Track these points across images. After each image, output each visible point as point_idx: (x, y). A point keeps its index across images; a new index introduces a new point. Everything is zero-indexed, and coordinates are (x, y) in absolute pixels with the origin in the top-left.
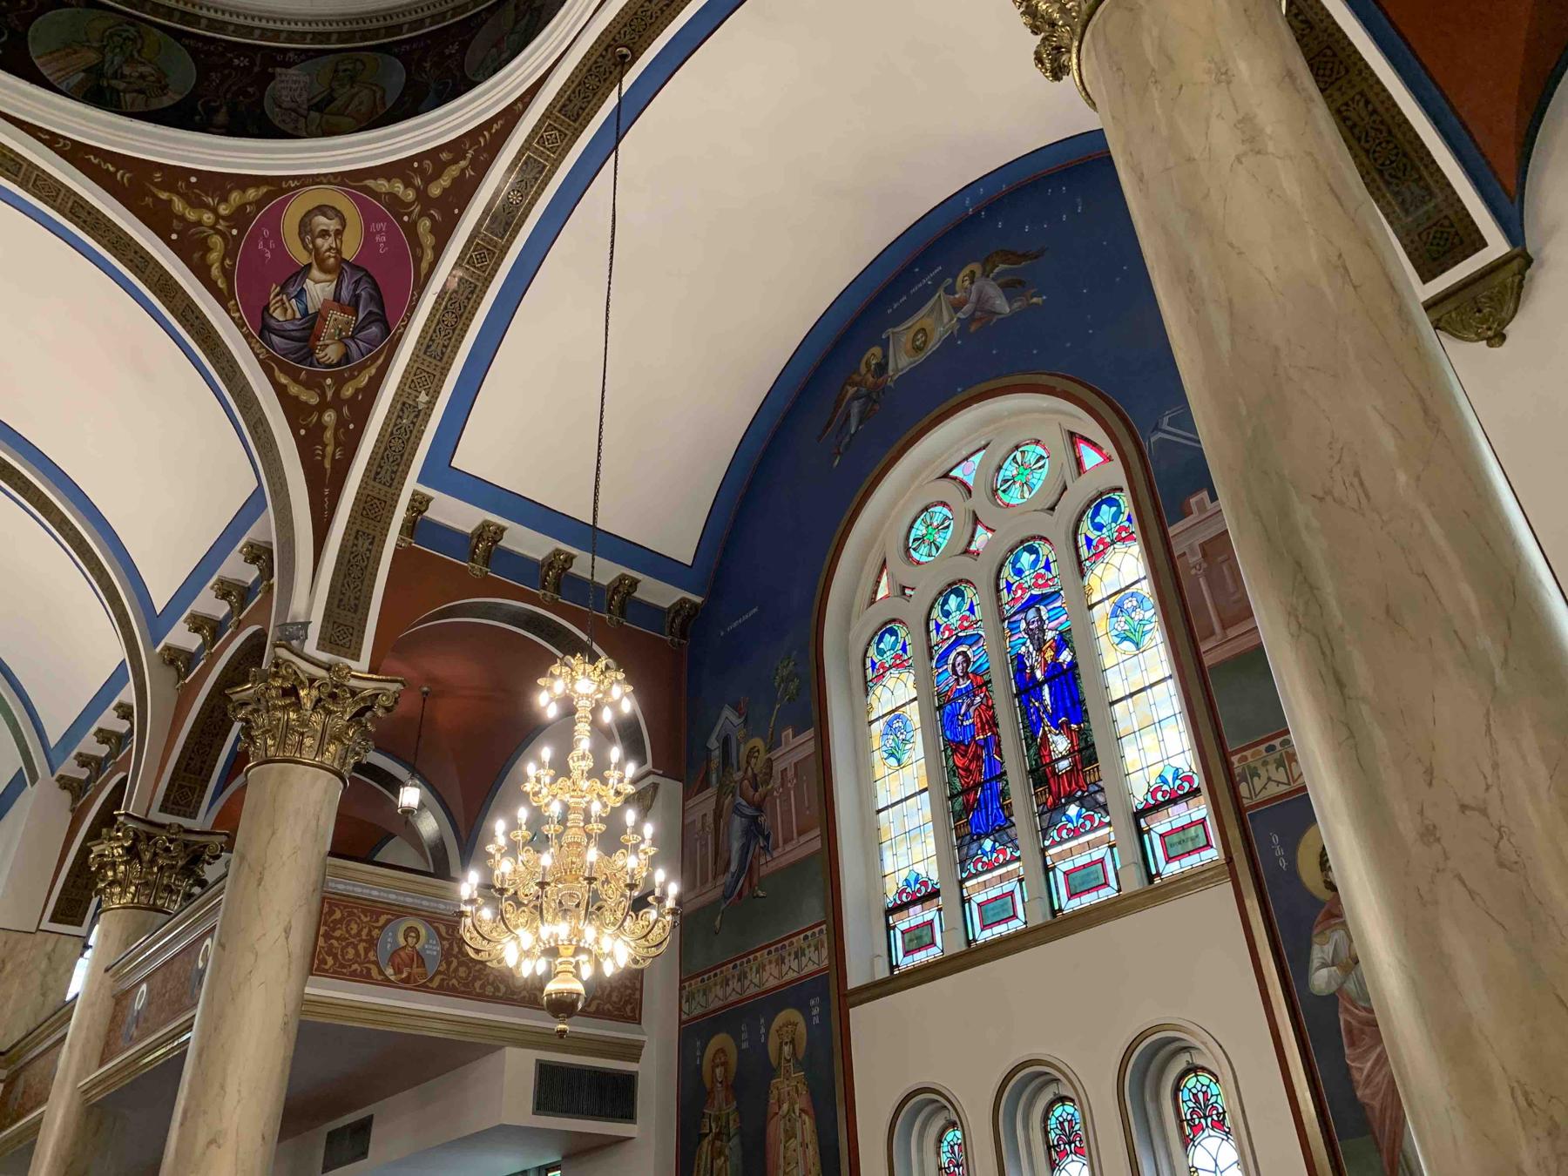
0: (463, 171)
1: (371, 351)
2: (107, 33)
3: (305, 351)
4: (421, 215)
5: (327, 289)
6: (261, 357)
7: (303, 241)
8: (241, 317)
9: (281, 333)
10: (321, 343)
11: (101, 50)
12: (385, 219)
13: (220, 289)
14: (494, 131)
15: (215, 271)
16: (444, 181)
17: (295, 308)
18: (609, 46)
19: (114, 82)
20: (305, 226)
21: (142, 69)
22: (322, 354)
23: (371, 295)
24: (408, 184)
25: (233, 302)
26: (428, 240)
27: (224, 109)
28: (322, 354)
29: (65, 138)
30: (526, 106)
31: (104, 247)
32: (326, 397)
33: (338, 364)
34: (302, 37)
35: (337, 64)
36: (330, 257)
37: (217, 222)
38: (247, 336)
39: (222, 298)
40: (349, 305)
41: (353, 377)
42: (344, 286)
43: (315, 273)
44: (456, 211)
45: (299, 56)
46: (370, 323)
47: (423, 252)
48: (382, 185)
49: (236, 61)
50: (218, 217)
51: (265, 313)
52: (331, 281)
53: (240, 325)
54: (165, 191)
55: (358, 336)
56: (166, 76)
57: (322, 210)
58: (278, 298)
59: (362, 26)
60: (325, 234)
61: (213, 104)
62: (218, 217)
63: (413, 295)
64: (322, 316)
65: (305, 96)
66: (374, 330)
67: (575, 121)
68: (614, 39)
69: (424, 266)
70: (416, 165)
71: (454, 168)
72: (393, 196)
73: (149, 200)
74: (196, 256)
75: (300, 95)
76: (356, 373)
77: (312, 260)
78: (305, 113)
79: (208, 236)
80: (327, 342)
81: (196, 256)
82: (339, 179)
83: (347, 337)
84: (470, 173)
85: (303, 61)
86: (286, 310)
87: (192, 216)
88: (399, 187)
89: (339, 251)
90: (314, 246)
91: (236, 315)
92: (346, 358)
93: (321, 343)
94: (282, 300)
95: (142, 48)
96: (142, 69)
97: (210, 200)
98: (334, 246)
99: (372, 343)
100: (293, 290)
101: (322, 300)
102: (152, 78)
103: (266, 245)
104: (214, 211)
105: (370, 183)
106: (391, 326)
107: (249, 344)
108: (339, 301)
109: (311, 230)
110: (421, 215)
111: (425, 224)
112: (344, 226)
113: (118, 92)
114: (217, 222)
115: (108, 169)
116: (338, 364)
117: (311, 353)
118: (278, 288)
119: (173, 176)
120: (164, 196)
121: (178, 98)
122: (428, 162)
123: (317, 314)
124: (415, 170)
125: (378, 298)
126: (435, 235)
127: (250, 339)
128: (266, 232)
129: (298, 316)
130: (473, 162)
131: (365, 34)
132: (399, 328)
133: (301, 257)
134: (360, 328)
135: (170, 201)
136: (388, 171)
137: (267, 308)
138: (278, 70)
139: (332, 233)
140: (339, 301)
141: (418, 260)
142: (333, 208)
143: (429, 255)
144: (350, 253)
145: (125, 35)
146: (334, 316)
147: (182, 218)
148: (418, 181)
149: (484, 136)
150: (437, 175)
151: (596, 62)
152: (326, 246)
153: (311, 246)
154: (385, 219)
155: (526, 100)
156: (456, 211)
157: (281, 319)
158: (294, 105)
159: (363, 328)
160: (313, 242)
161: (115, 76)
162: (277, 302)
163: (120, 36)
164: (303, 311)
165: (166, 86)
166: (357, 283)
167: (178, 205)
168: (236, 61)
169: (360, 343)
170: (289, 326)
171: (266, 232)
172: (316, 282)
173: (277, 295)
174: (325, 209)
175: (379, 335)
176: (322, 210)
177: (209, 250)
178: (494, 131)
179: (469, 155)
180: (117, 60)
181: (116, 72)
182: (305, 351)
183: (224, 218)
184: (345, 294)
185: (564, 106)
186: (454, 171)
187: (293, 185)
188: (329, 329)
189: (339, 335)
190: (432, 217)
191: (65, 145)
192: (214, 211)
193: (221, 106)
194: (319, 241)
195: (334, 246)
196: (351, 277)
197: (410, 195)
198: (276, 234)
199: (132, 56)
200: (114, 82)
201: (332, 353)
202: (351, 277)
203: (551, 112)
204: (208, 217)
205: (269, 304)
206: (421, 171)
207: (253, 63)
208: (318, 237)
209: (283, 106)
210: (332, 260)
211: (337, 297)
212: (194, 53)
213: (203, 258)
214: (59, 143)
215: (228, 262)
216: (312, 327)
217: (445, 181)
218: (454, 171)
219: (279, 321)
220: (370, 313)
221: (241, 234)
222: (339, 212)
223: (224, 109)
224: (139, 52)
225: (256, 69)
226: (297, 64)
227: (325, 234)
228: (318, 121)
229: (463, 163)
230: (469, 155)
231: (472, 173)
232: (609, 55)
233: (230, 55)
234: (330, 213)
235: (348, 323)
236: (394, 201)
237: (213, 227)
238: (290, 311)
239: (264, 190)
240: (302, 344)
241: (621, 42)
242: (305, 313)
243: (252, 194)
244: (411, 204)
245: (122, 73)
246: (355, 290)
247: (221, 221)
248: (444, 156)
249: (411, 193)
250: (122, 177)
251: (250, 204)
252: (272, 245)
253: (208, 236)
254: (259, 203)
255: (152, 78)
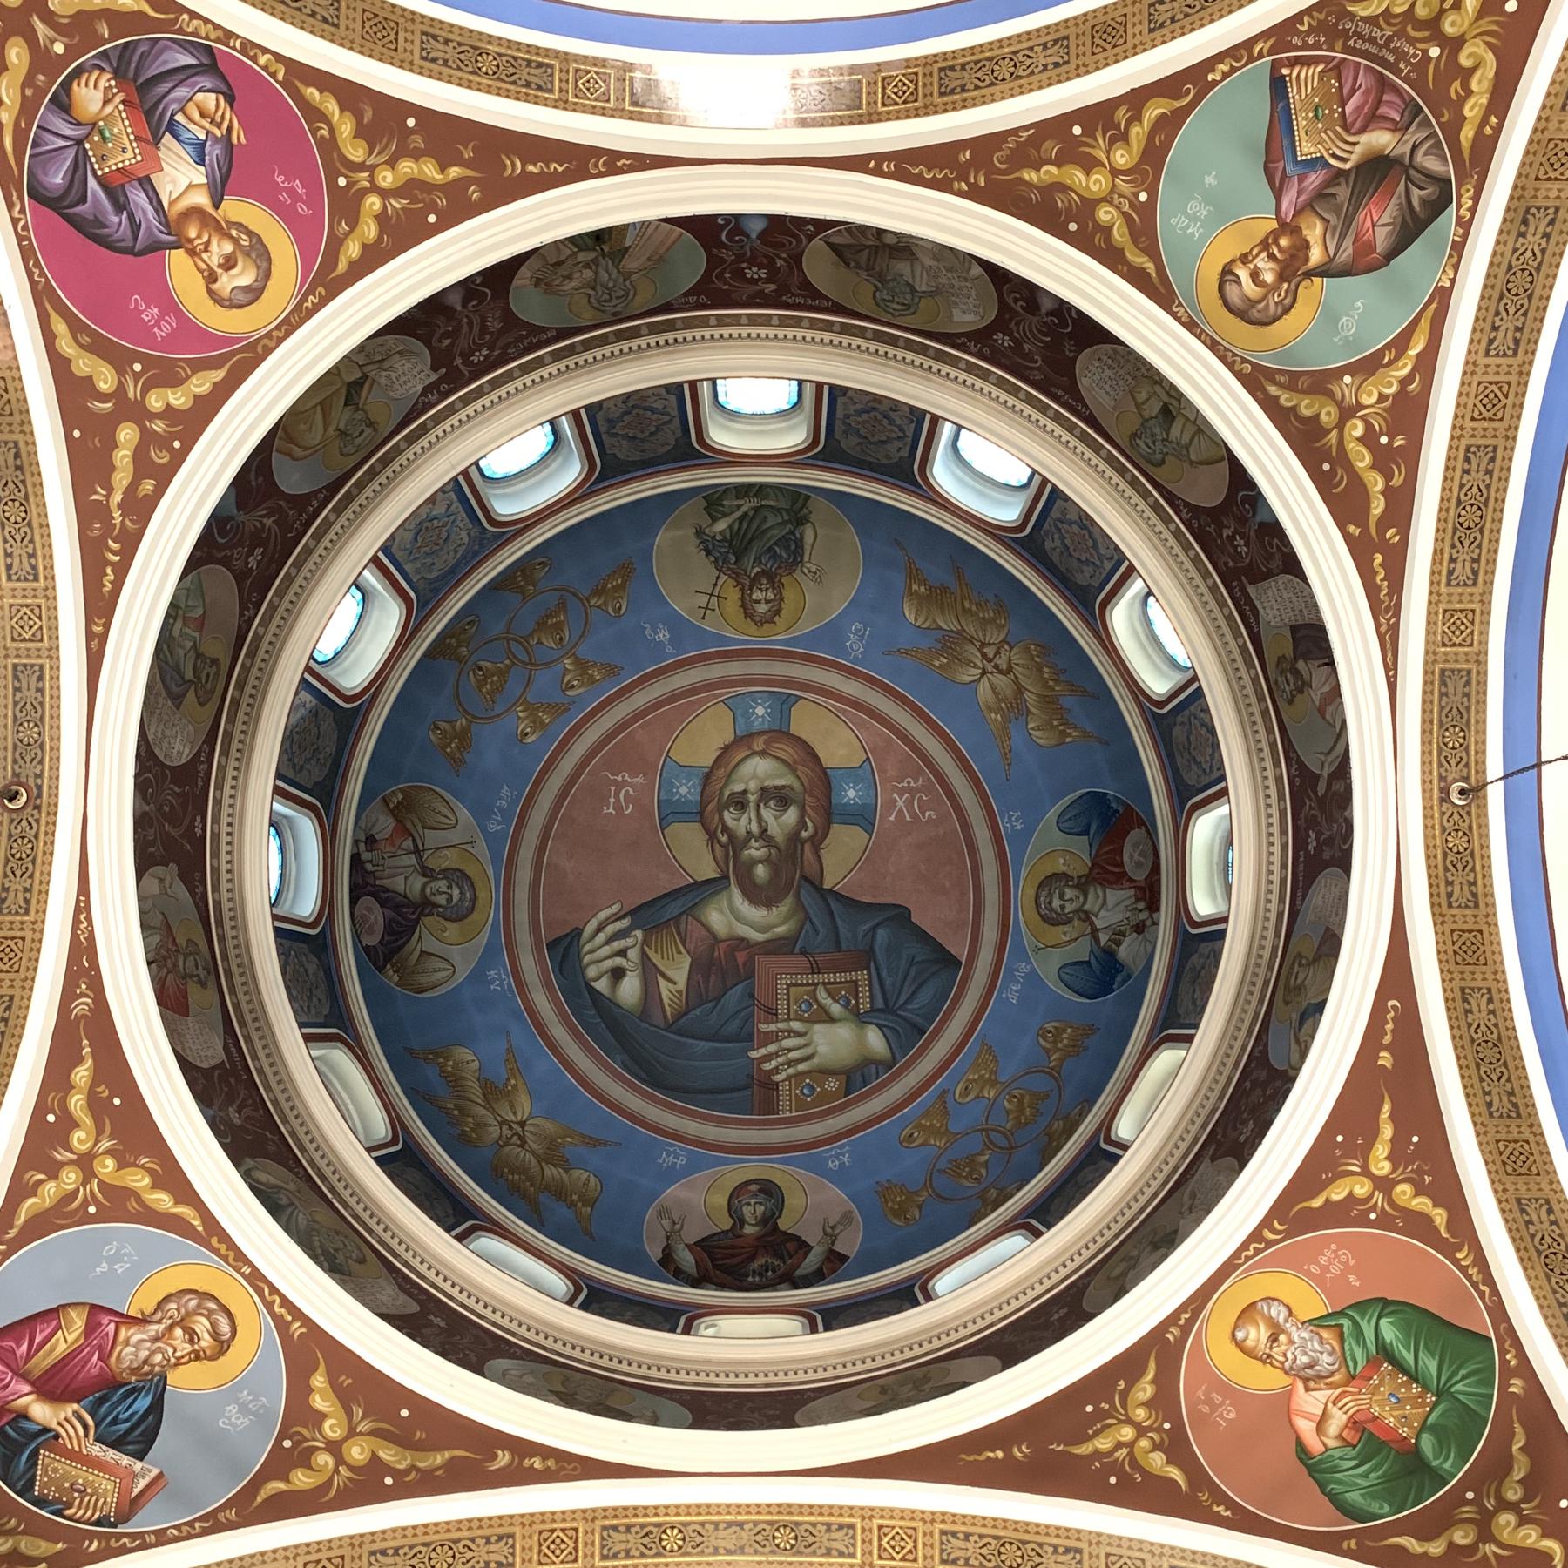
0: (110, 490)
1: (35, 145)
2: (632, 292)
3: (131, 74)
4: (121, 388)
5: (169, 187)
6: (185, 16)
7: (250, 233)
8: (254, 59)
9: (181, 74)
10: (118, 99)
11: (627, 276)
12: (166, 345)
13: (308, 85)
14: (109, 570)
15: (331, 106)
16: (123, 457)
17: (191, 127)
18: (39, 796)
19: (592, 255)
20: (259, 253)
21: (574, 284)
22: (102, 83)
23: (104, 226)
24: (169, 412)
25: (280, 76)
26: (84, 364)
27: (459, 308)
28: (102, 83)
29: (601, 175)
30: (90, 635)
31: (490, 39)
32: (42, 20)
33: (66, 86)
34: (438, 419)
35: (375, 430)
36: (199, 236)
37: (372, 180)
38: (228, 35)
39: (299, 73)
40: (122, 186)
41: (28, 81)
42: (150, 210)
43: (202, 199)
44: (77, 434)
45: (424, 403)
46: (72, 181)
47: (76, 341)
48: (201, 384)
49: (485, 352)
50: (375, 189)
51: (225, 89)
52: (171, 204)
53: (248, 47)
54: (456, 181)
55: (73, 151)
56: (545, 292)
57: (254, 293)
58: (225, 126)
59: (383, 479)
60: (229, 263)
61: (475, 303)
62: (375, 189)
63: (42, 274)
64: (146, 141)
65: (383, 381)
66: (57, 178)
67: (15, 666)
68: (38, 807)
69: (60, 327)
70: (177, 444)
71: (125, 483)
72: (176, 382)
73: (468, 154)
74: (368, 115)
75: (388, 377)
76: (29, 92)
77: (219, 215)
78: (366, 369)
79: (371, 153)
80: (109, 109)
81: (368, 115)
82: (260, 350)
83: (87, 136)
84: (99, 495)
85: (417, 402)
86: (203, 115)
87: (407, 167)
88: (178, 399)
89: (192, 253)
90: (231, 237)
91: (263, 59)
92: (62, 103)
93: (118, 99)
94: (219, 126)
95: (589, 302)
96: (574, 284)
97: (398, 206)
98: (205, 256)
99: (43, 158)
100: (213, 152)
101: (164, 165)
102: (557, 282)
103: (291, 192)
104: (384, 194)
105: (218, 375)
106: (120, 48)
107: (216, 27)
108: (140, 181)
109: (248, 255)
110: (121, 388)
111: (106, 379)
112: (211, 292)
113: (581, 250)
114: (372, 180)
115: (535, 164)
116: (66, 86)
117: (117, 74)
118: (235, 140)
119: (458, 209)
120: (454, 172)
121: (516, 283)
122: (165, 460)
123: (157, 140)
124: (173, 436)
125: (91, 230)
126: (82, 378)
127: (220, 33)
128: (303, 209)
129: (179, 117)
130: (103, 510)
131: (373, 474)
132: (22, 211)
133: (237, 209)
134: (80, 165)
135: (443, 169)
136: (206, 408)
137: (230, 99)
138: (434, 377)
139: (219, 271)
140: (140, 181)
141: (75, 326)
142: (240, 307)
143: (66, 346)
144: (178, 265)
145: (614, 302)
146: (130, 154)
147: (416, 155)
148: (158, 426)
149: (115, 553)
150: (140, 455)
151: (41, 762)
152: (214, 246)
153: (234, 233)
154: (166, 345)
155: (95, 643)
156: (77, 434)
157: (200, 96)
158: (386, 365)
159: (75, 165)
160: (235, 241)
161: (595, 261)
162: (223, 116)
163: (617, 298)
164: (180, 130)
165: (536, 285)
166: (135, 227)
167: (429, 170)
168: (485, 352)
169: (62, 143)
170: (181, 92)
171: (303, 209)
172: (190, 186)
173: (230, 129)
174: (250, 297)
175: (42, 177)
176: (254, 293)
177: (358, 134)
178: (109, 570)
179: (117, 514)
180: (604, 276)
181: (597, 265)
182: (131, 74)
183: (364, 192)
184: (139, 198)
185: (41, 678)
186: (121, 479)
187: (311, 297)
188: (122, 129)
189: (101, 133)
190: (104, 397)
191: (596, 166)
192: (384, 194)
193: (464, 306)
194: (228, 248)
195: (205, 256)
196: (149, 228)
197: (155, 402)
198: (286, 214)
199: (593, 289)
200: (592, 255)
201: (91, 96)
202: (149, 228)
203: (50, 658)
204: (386, 178)
205: (231, 107)
206: (163, 442)
207: (467, 363)
208: (233, 252)
209: (397, 357)
210: (192, 234)
211: (147, 184)
212: (536, 330)
213: (359, 116)
214: (604, 164)
215: (324, 132)
216: (149, 114)
217: (123, 457)
218: (121, 479)
219: (199, 91)
220: (83, 200)
221: (332, 182)
222: (230, 307)
223: (459, 308)
224: (589, 296)
225: (458, 361)
226: (420, 396)
227: (229, 263)
228: (344, 376)
229: (117, 497)
230: (117, 514)
231: (95, 497)
232: (31, 782)
233: (496, 353)
234: (241, 297)
235: (102, 159)
236: (168, 376)
237: (372, 169)
238: (196, 116)
239: (342, 266)
240: (141, 81)
241: (29, 810)
242: (172, 128)
243: (353, 250)
244: (145, 391)
245: (590, 268)
246: (131, 216)
247: (367, 185)
248: (148, 486)
249: (158, 405)
250: (513, 165)
251: (347, 235)
252: (284, 197)
253: (371, 153)
254: (336, 244)
255: (557, 282)
